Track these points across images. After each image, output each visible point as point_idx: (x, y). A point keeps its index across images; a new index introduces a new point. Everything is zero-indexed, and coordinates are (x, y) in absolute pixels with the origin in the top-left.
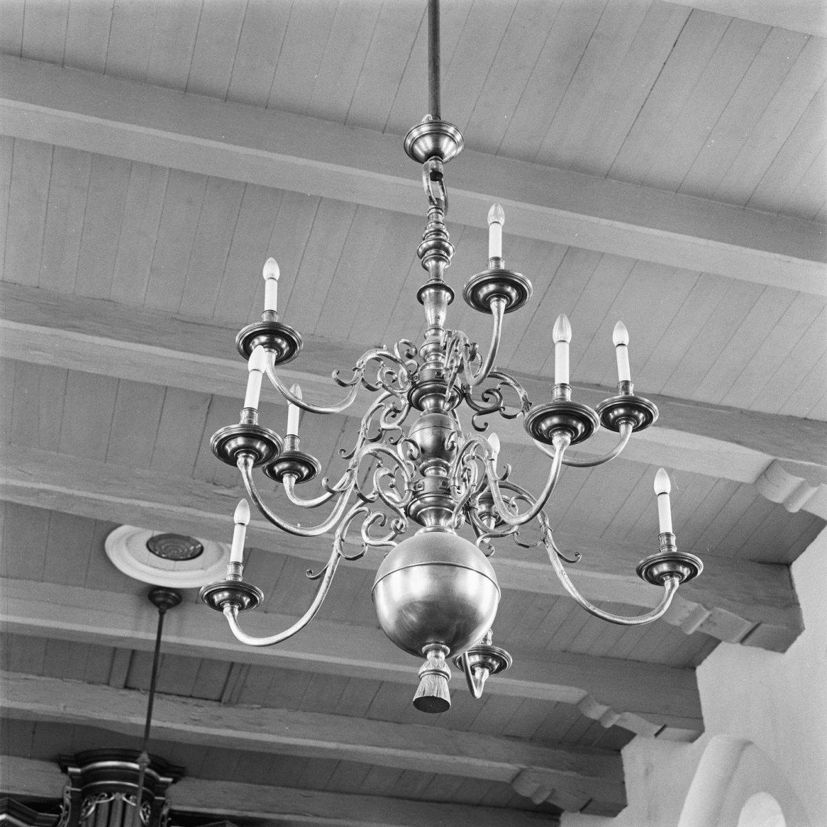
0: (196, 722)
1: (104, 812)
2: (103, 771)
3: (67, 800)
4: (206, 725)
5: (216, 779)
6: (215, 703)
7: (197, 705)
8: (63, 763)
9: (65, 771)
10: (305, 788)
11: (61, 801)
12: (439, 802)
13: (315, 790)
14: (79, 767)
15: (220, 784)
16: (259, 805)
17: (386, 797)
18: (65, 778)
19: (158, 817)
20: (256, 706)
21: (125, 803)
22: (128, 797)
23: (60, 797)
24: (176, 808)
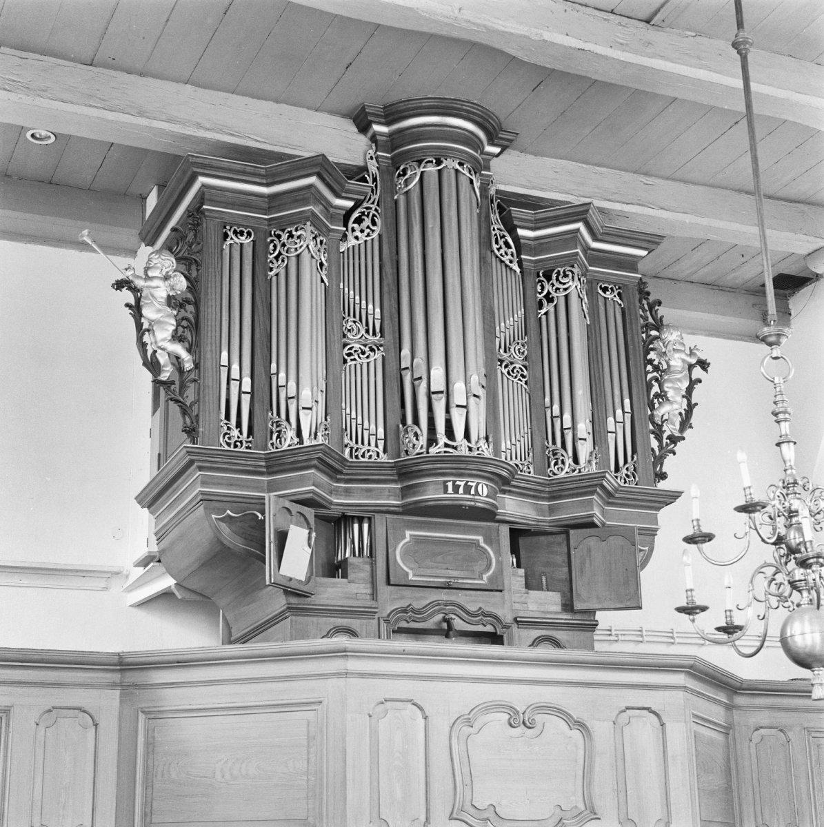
0: (622, 46)
1: (432, 183)
2: (414, 130)
3: (373, 167)
4: (636, 52)
5: (542, 155)
6: (643, 24)
7: (620, 24)
8: (362, 122)
9: (363, 128)
10: (646, 174)
11: (365, 169)
12: (791, 201)
13: (657, 176)
14: (388, 124)
15: (549, 161)
16: (596, 190)
17: (736, 191)
18: (363, 140)
19: (487, 197)
20: (690, 33)
21: (457, 171)
22: (461, 164)
23: (361, 163)
24: (502, 187)
